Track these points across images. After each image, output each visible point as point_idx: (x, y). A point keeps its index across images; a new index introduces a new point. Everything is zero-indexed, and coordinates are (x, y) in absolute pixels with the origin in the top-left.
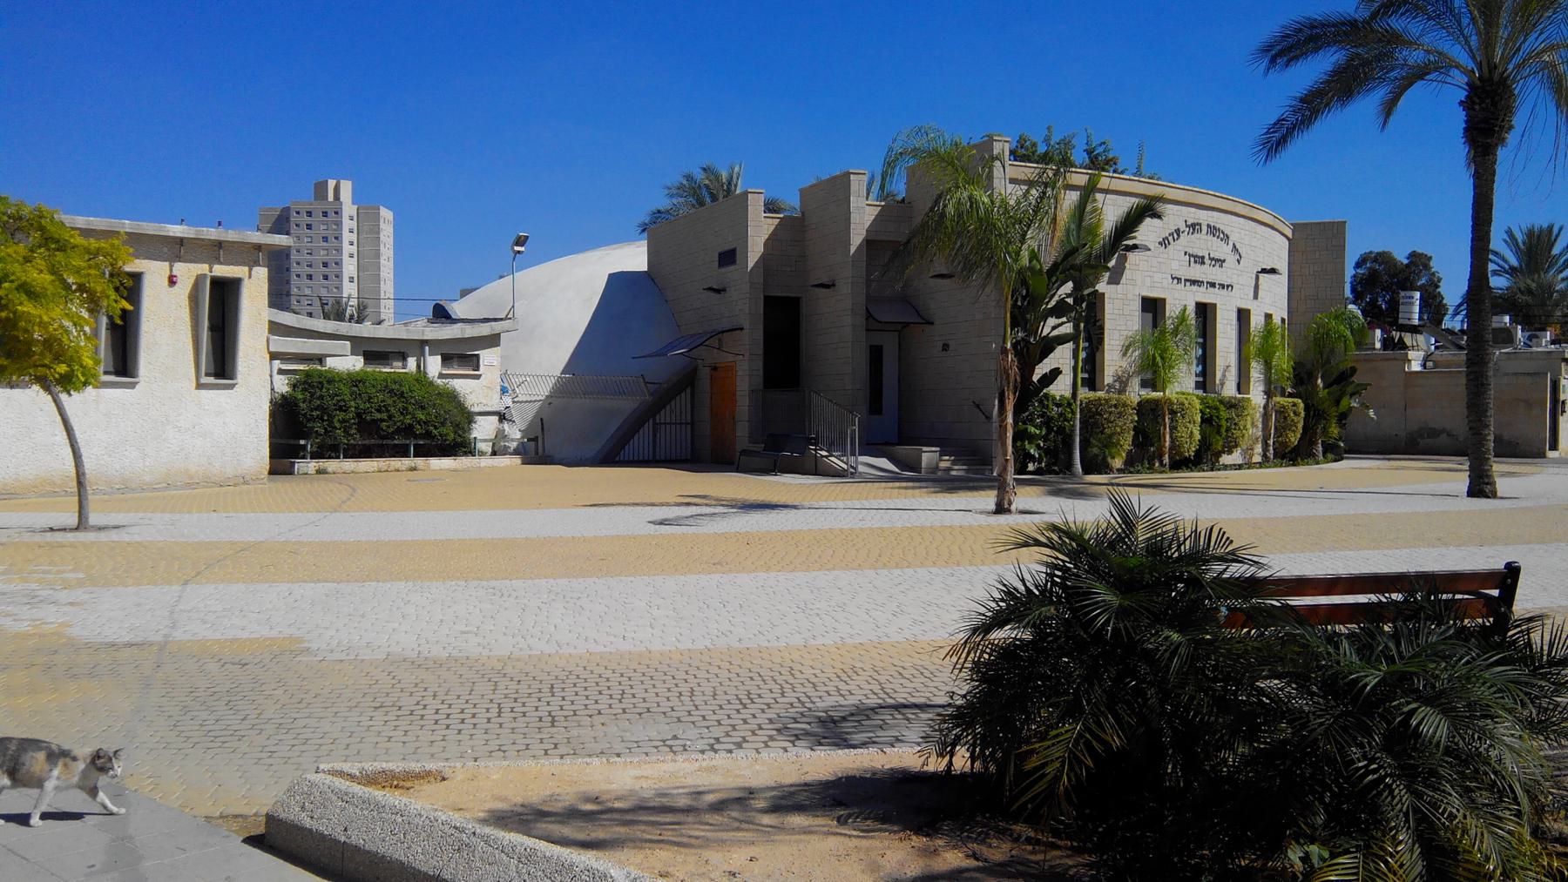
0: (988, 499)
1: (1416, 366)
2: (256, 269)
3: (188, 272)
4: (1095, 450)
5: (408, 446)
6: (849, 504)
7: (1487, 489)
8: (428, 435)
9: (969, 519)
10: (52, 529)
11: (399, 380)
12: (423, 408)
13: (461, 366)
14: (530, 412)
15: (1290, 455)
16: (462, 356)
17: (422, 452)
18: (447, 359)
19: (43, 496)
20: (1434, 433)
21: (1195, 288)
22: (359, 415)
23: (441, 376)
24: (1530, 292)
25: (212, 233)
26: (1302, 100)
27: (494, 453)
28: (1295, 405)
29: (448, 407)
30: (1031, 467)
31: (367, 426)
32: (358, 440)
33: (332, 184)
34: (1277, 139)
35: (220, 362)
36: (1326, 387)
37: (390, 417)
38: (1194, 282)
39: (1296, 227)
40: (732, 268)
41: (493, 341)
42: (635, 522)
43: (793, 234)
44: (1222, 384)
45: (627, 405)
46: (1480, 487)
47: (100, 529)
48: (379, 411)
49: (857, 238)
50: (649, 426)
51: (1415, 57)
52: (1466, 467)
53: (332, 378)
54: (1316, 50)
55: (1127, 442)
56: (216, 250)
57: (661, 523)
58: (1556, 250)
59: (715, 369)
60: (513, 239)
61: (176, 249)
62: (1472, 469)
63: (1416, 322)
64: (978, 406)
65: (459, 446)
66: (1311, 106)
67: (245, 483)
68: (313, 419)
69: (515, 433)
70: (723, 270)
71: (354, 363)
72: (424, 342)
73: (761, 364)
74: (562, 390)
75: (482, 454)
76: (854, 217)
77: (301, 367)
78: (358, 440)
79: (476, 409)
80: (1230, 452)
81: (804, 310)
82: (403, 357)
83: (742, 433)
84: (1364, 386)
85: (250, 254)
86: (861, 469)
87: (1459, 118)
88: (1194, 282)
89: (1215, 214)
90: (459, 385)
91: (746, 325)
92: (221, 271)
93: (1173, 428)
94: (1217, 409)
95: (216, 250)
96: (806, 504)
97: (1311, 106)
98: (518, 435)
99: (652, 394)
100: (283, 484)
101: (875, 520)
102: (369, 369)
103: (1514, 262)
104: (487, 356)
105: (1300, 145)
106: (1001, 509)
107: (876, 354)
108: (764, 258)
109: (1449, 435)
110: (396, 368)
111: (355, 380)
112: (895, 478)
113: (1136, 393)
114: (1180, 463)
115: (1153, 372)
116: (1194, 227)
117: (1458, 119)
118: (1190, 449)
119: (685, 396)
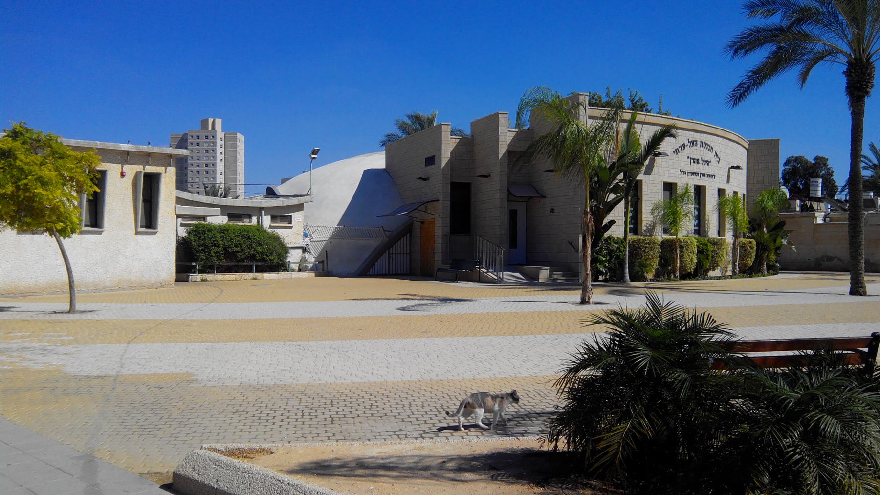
0: (576, 296)
1: (820, 221)
2: (169, 168)
3: (131, 170)
4: (637, 269)
5: (251, 267)
7: (861, 290)
8: (263, 260)
9: (565, 307)
11: (247, 229)
12: (260, 245)
14: (320, 247)
15: (748, 271)
16: (282, 216)
17: (260, 270)
18: (274, 218)
20: (830, 259)
21: (694, 177)
22: (225, 249)
23: (271, 227)
25: (145, 148)
26: (754, 73)
27: (300, 270)
28: (750, 243)
29: (275, 244)
30: (601, 278)
31: (229, 255)
32: (224, 263)
33: (211, 120)
34: (740, 94)
35: (149, 219)
37: (242, 250)
38: (693, 174)
39: (751, 143)
40: (433, 166)
41: (299, 207)
42: (390, 308)
45: (374, 243)
46: (857, 289)
47: (82, 312)
48: (236, 246)
49: (503, 150)
50: (386, 255)
52: (849, 277)
53: (210, 229)
56: (146, 158)
57: (403, 309)
59: (423, 223)
60: (311, 151)
61: (125, 157)
62: (852, 279)
63: (820, 196)
65: (280, 266)
67: (162, 287)
68: (200, 251)
69: (311, 259)
72: (261, 208)
73: (449, 220)
74: (337, 235)
75: (293, 270)
76: (501, 138)
78: (224, 263)
79: (290, 246)
80: (714, 270)
81: (473, 189)
82: (250, 217)
83: (438, 258)
85: (165, 160)
87: (843, 81)
88: (693, 174)
89: (705, 135)
90: (281, 232)
91: (441, 199)
92: (150, 169)
93: (682, 256)
95: (146, 158)
97: (759, 77)
98: (313, 260)
100: (183, 287)
101: (513, 308)
103: (875, 162)
104: (296, 216)
105: (753, 97)
106: (584, 302)
107: (513, 215)
108: (450, 161)
109: (839, 260)
110: (246, 223)
111: (223, 230)
116: (693, 143)
118: (691, 268)
119: (405, 240)
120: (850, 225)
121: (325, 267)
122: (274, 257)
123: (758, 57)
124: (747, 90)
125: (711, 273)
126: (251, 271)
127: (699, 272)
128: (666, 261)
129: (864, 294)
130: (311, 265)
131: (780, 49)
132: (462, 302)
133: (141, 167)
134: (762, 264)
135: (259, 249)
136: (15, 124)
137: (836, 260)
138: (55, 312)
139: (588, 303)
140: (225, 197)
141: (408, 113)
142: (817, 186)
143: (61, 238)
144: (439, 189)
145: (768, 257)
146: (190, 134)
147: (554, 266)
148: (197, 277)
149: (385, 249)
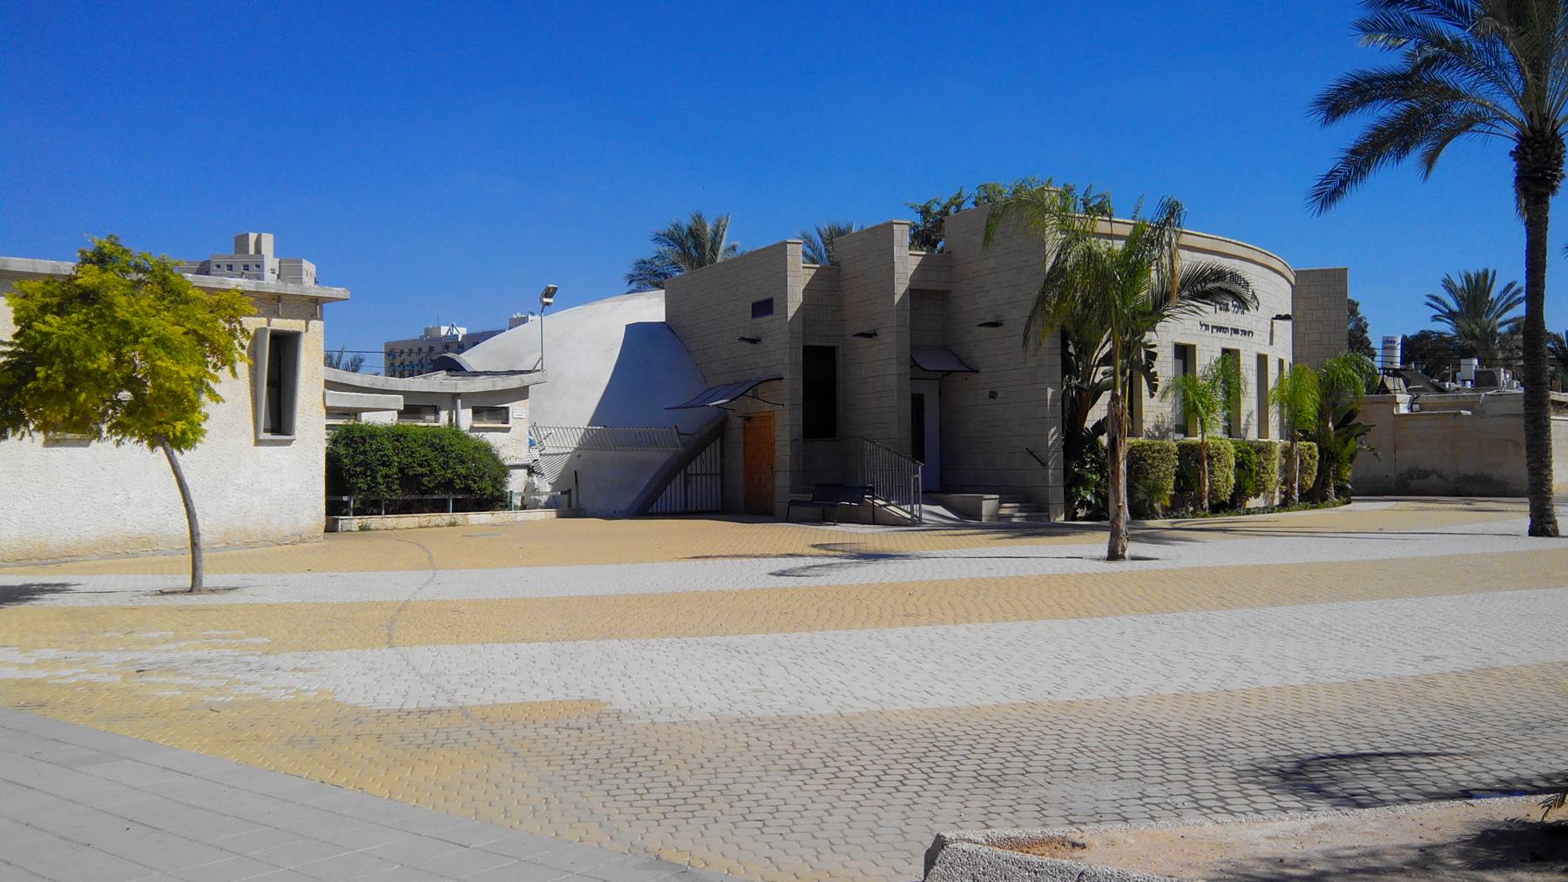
0: (1098, 543)
1: (1403, 409)
2: (313, 323)
4: (1141, 496)
5: (445, 501)
6: (958, 552)
7: (1550, 528)
8: (467, 489)
10: (162, 593)
11: (437, 433)
12: (463, 462)
13: (490, 419)
14: (559, 464)
15: (1313, 498)
16: (492, 408)
17: (461, 507)
18: (477, 412)
19: (103, 558)
20: (1425, 474)
22: (401, 470)
23: (472, 429)
24: (1473, 336)
26: (1353, 152)
27: (524, 507)
28: (1310, 448)
30: (1081, 513)
31: (409, 481)
32: (399, 495)
33: (253, 237)
34: (1331, 191)
35: (278, 418)
36: (1336, 428)
37: (431, 472)
38: (1220, 329)
39: (1298, 274)
40: (769, 318)
41: (521, 393)
42: (751, 575)
43: (831, 281)
44: (1246, 430)
45: (659, 457)
47: (213, 591)
48: (421, 466)
49: (901, 287)
50: (680, 478)
51: (1458, 110)
52: (1527, 508)
53: (372, 433)
54: (1363, 103)
55: (1170, 485)
57: (782, 574)
58: (1494, 294)
59: (749, 419)
60: (542, 290)
63: (1398, 366)
64: (1032, 453)
65: (495, 501)
66: (1363, 158)
67: (303, 541)
68: (356, 475)
69: (544, 486)
70: (758, 320)
71: (387, 419)
72: (456, 396)
74: (590, 443)
76: (898, 266)
77: (341, 422)
78: (399, 495)
79: (507, 463)
80: (1257, 496)
81: (840, 359)
82: (435, 411)
83: (782, 482)
84: (1369, 428)
86: (924, 516)
87: (1510, 166)
88: (1220, 329)
89: (1237, 261)
90: (490, 438)
91: (786, 375)
92: (280, 324)
93: (1211, 472)
94: (1248, 453)
96: (920, 552)
97: (1363, 158)
98: (548, 489)
99: (684, 445)
100: (334, 541)
101: (977, 570)
102: (407, 423)
103: (1455, 307)
104: (517, 409)
105: (1356, 198)
106: (1114, 555)
107: (918, 402)
109: (1440, 476)
110: (427, 422)
111: (396, 435)
112: (957, 527)
113: (1174, 441)
114: (1218, 508)
115: (1189, 416)
117: (1507, 170)
118: (1226, 494)
119: (714, 448)
120: (1527, 415)
121: (573, 501)
122: (486, 484)
123: (1357, 125)
124: (1343, 184)
125: (1252, 503)
126: (444, 509)
127: (1233, 504)
128: (1187, 481)
129: (1554, 533)
130: (544, 498)
131: (1404, 118)
132: (883, 561)
133: (264, 320)
134: (1328, 486)
135: (461, 470)
136: (95, 240)
137: (1433, 478)
138: (162, 593)
139: (1123, 557)
140: (355, 371)
141: (665, 227)
142: (1394, 348)
143: (176, 453)
144: (781, 357)
145: (1338, 475)
146: (215, 261)
147: (1006, 496)
148: (351, 522)
149: (676, 468)
